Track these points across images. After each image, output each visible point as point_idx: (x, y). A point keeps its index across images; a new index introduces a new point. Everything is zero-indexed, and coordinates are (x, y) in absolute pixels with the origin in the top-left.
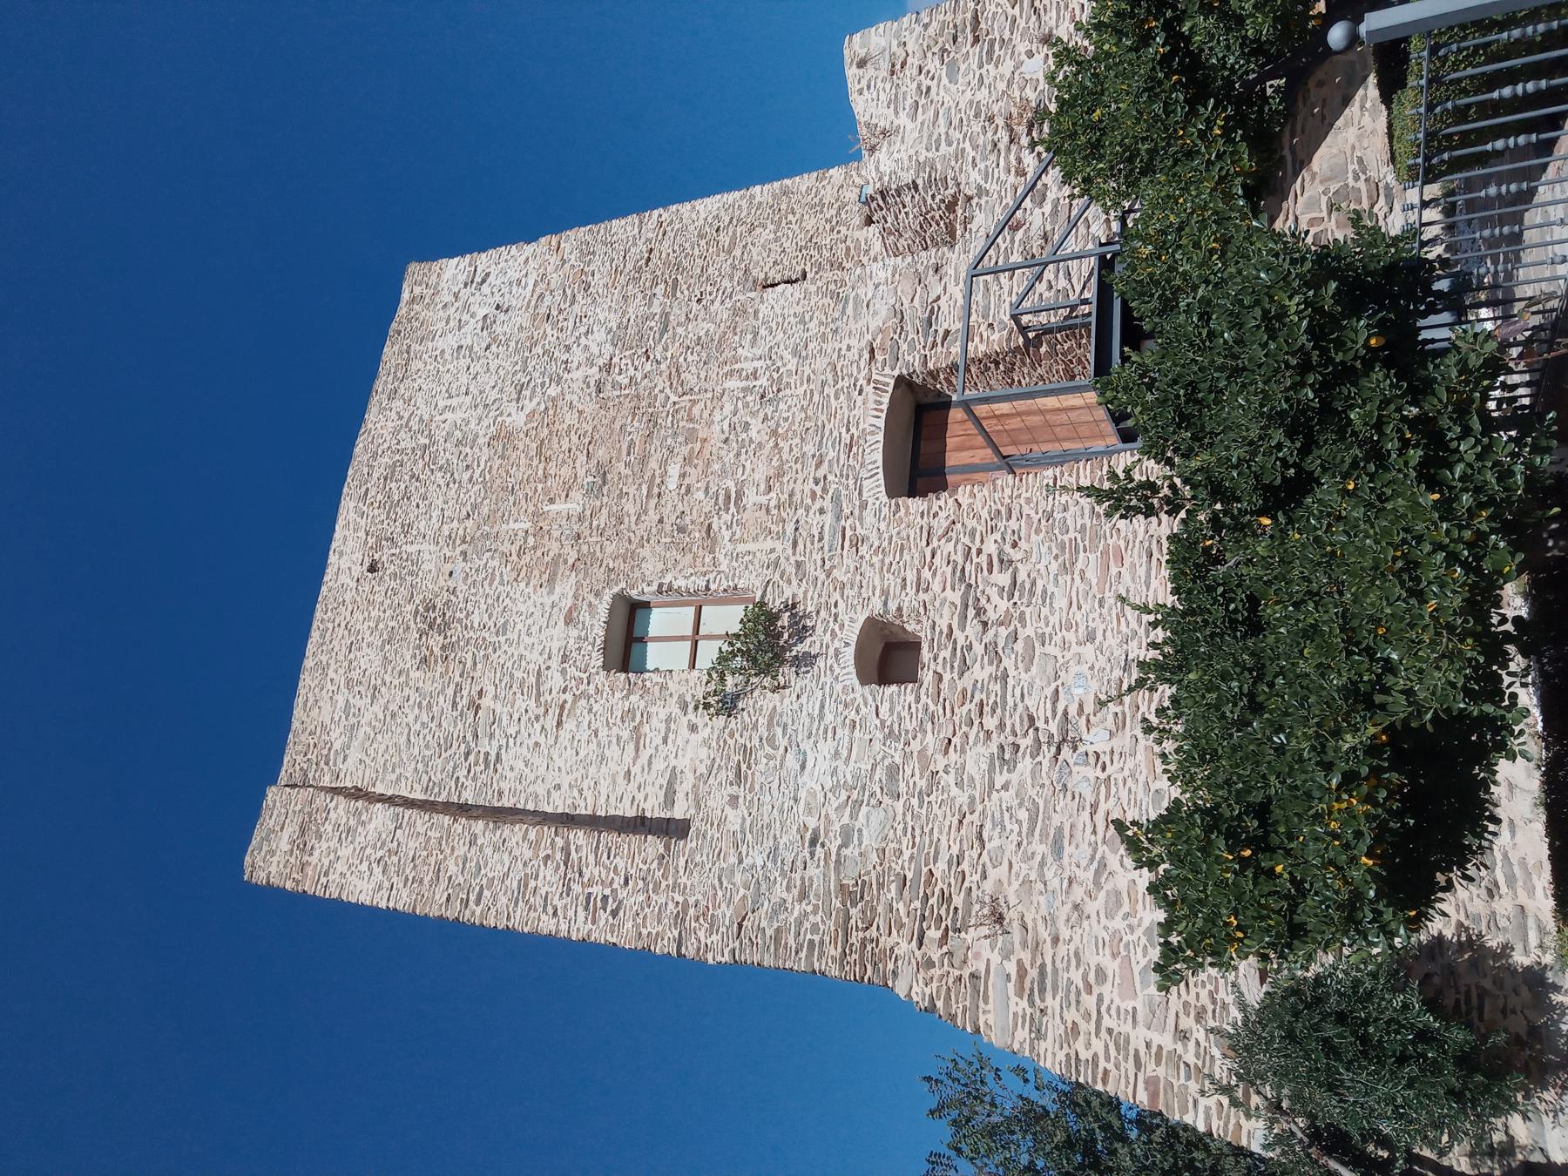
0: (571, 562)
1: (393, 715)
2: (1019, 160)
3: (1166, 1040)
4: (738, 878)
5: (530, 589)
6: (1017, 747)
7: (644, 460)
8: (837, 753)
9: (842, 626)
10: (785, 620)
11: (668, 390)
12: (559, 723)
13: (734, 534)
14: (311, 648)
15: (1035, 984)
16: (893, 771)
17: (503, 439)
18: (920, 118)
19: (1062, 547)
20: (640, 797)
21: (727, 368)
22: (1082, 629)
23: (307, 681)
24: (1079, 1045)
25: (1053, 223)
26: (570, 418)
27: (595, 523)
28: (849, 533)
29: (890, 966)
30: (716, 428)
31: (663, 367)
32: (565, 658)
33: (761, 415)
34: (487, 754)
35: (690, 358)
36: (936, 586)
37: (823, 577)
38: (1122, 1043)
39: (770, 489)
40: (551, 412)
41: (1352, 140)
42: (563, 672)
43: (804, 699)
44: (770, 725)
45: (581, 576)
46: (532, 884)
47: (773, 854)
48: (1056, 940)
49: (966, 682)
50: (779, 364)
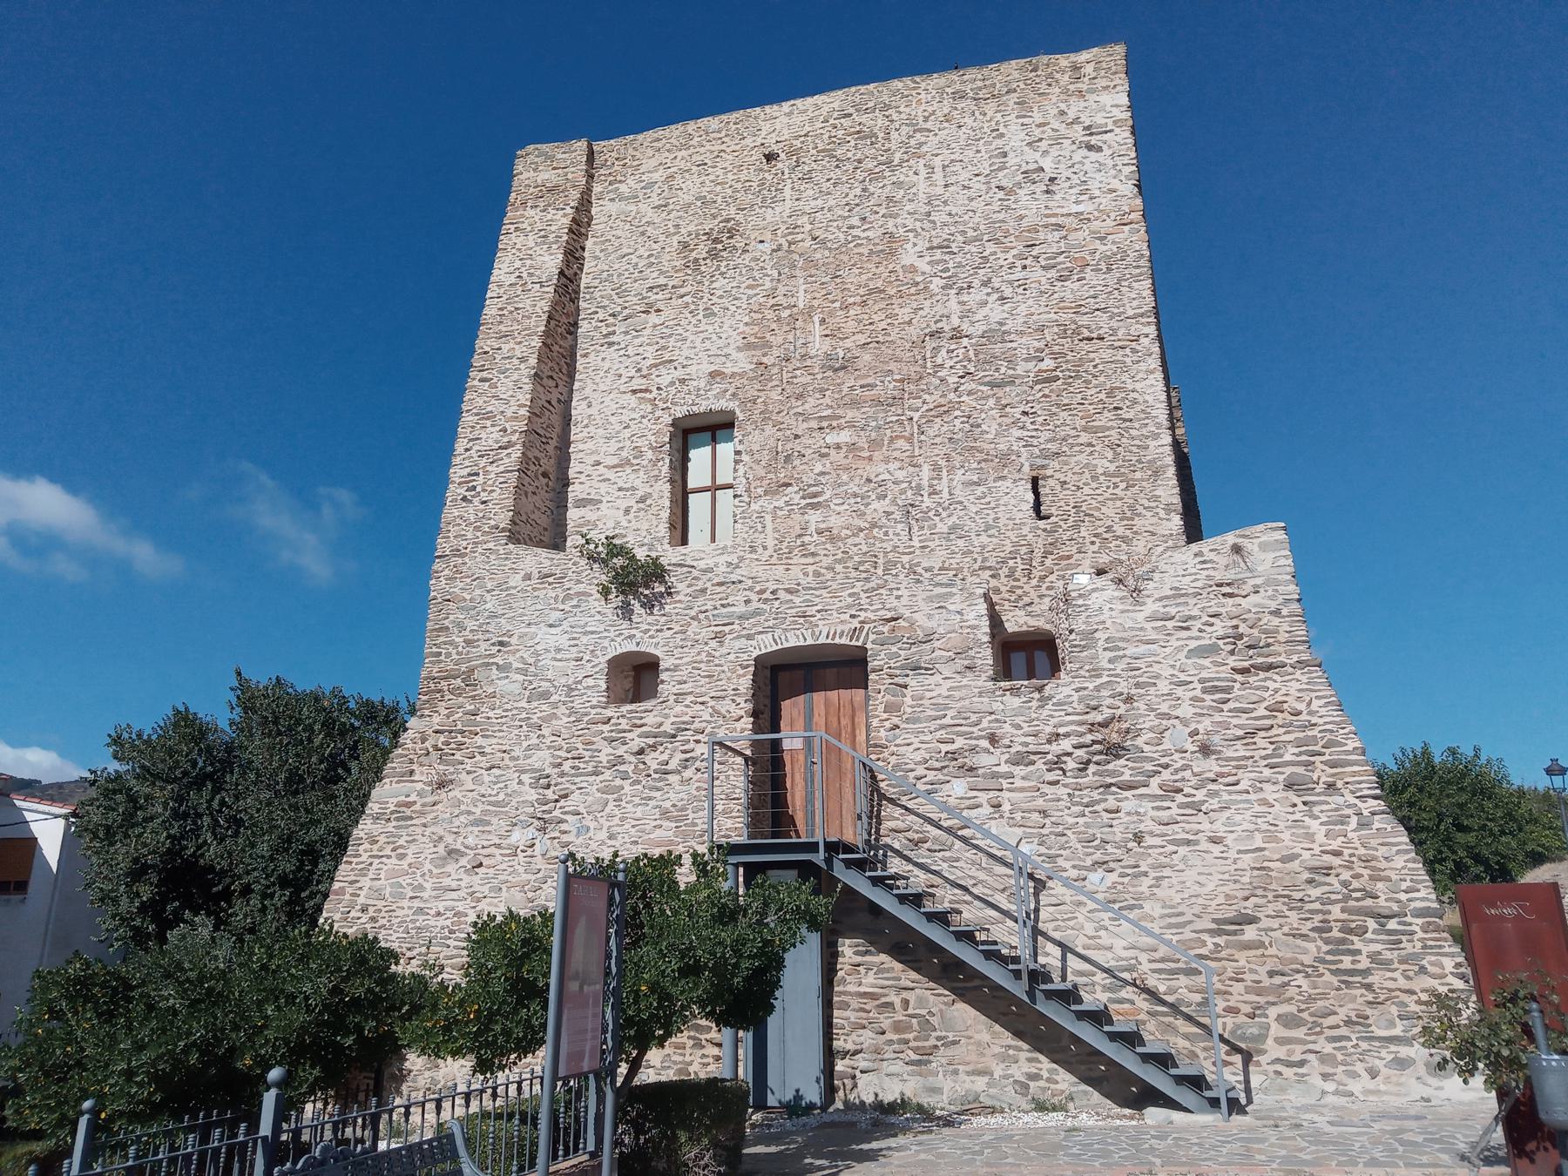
0: (765, 360)
1: (643, 234)
2: (1067, 735)
3: (361, 900)
4: (478, 592)
5: (742, 328)
6: (548, 787)
7: (855, 404)
8: (558, 650)
9: (652, 637)
10: (659, 588)
11: (926, 407)
12: (634, 392)
13: (781, 509)
14: (703, 122)
15: (403, 813)
16: (545, 695)
17: (891, 245)
18: (1148, 626)
19: (683, 809)
20: (583, 478)
21: (943, 463)
22: (619, 829)
23: (674, 132)
24: (367, 846)
25: (984, 776)
26: (904, 313)
27: (798, 373)
28: (727, 629)
29: (427, 712)
30: (882, 468)
31: (952, 396)
32: (682, 381)
33: (892, 509)
34: (614, 333)
35: (957, 422)
36: (679, 708)
37: (693, 613)
38: (363, 872)
39: (820, 533)
40: (913, 290)
41: (978, 1037)
42: (672, 383)
43: (598, 617)
44: (579, 594)
45: (751, 374)
46: (489, 423)
47: (494, 616)
48: (425, 825)
49: (600, 743)
50: (944, 514)
